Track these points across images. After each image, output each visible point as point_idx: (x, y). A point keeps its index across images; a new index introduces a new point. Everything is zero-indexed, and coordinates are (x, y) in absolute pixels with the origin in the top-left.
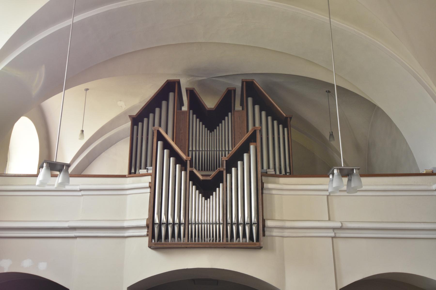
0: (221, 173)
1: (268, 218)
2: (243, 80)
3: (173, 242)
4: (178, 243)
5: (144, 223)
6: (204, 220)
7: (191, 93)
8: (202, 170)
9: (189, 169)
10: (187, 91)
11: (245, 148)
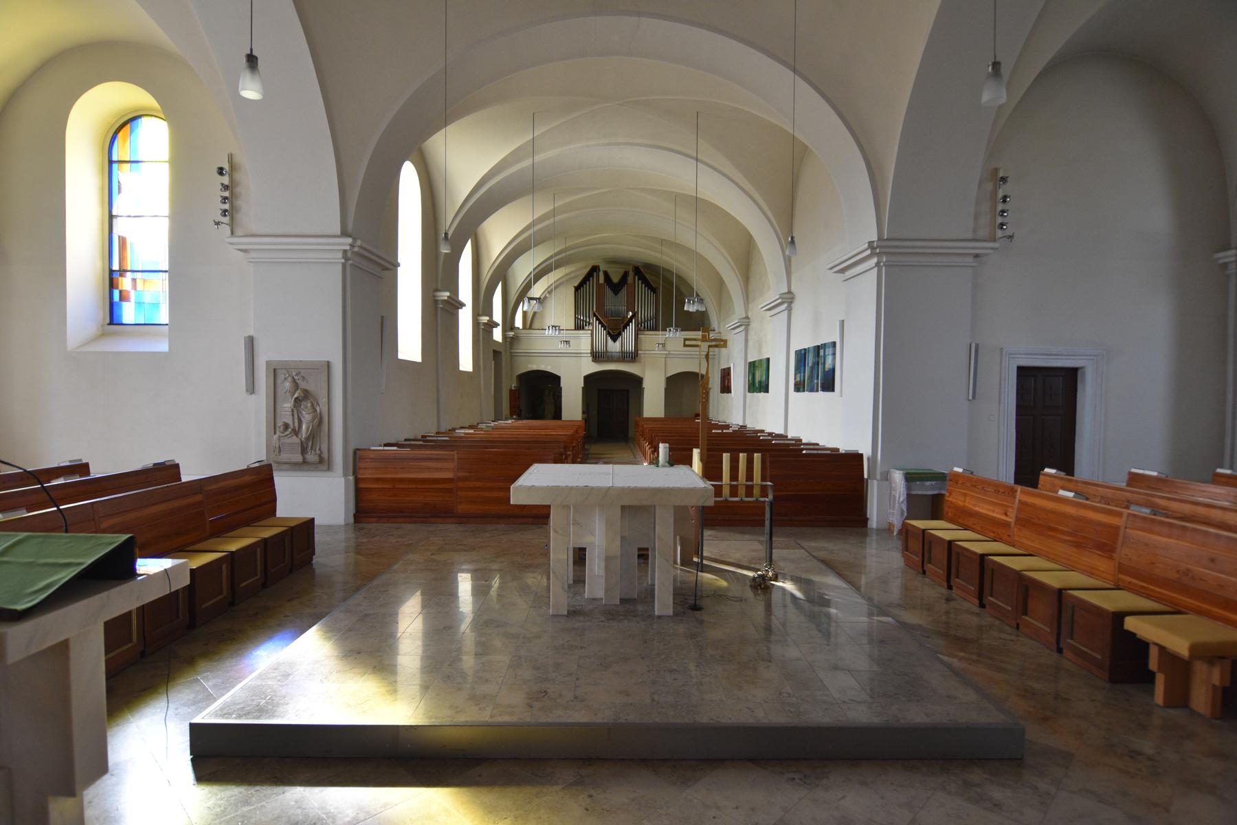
5: (590, 352)
7: (606, 273)
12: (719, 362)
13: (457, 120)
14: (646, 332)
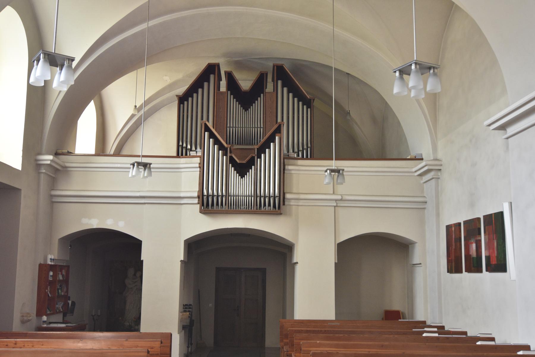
0: (253, 159)
1: (288, 192)
2: (274, 65)
3: (217, 208)
4: (221, 210)
5: (196, 194)
6: (240, 193)
7: (230, 76)
8: (238, 144)
9: (229, 155)
10: (225, 73)
11: (272, 139)
12: (438, 215)
13: (130, 72)
14: (300, 162)
